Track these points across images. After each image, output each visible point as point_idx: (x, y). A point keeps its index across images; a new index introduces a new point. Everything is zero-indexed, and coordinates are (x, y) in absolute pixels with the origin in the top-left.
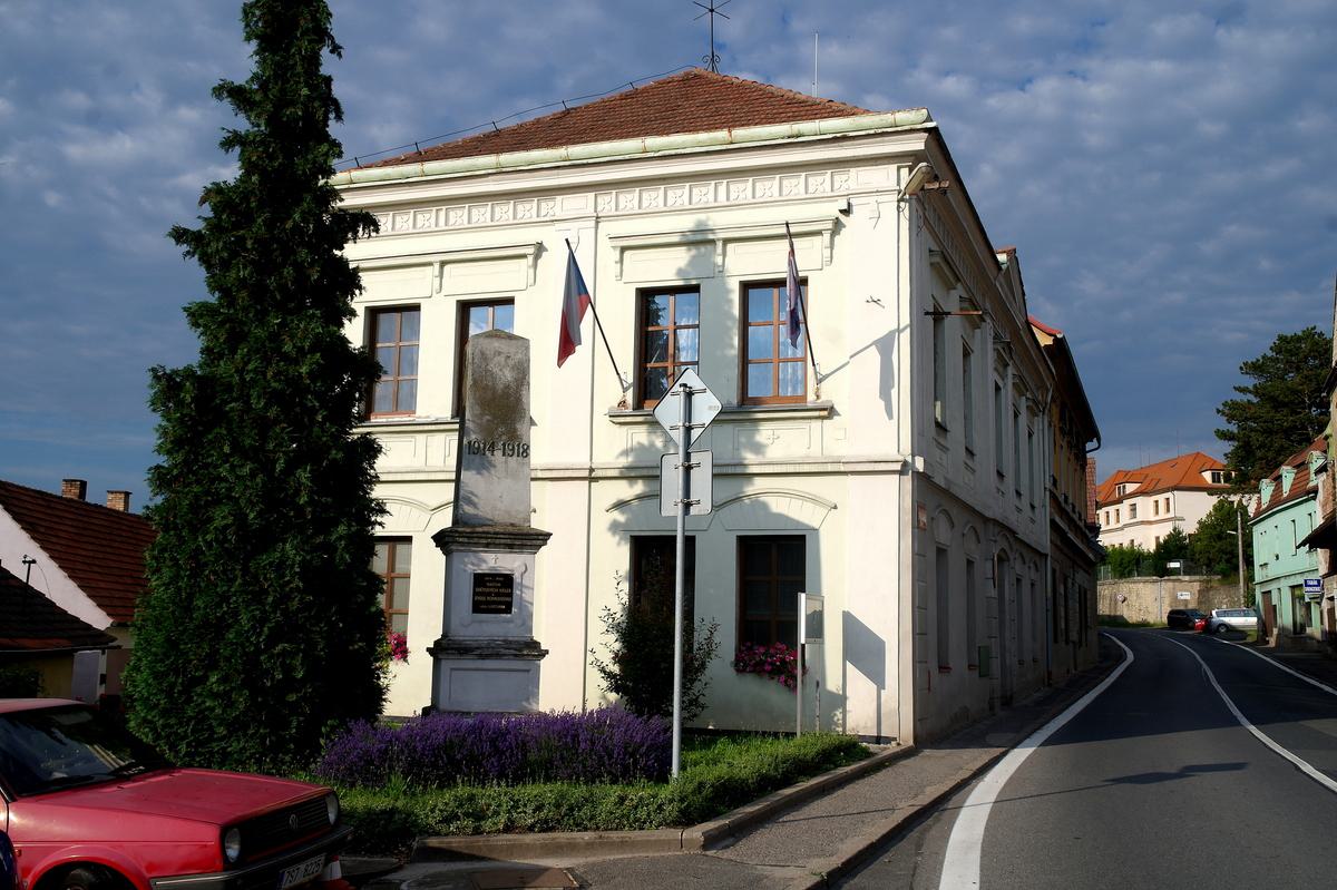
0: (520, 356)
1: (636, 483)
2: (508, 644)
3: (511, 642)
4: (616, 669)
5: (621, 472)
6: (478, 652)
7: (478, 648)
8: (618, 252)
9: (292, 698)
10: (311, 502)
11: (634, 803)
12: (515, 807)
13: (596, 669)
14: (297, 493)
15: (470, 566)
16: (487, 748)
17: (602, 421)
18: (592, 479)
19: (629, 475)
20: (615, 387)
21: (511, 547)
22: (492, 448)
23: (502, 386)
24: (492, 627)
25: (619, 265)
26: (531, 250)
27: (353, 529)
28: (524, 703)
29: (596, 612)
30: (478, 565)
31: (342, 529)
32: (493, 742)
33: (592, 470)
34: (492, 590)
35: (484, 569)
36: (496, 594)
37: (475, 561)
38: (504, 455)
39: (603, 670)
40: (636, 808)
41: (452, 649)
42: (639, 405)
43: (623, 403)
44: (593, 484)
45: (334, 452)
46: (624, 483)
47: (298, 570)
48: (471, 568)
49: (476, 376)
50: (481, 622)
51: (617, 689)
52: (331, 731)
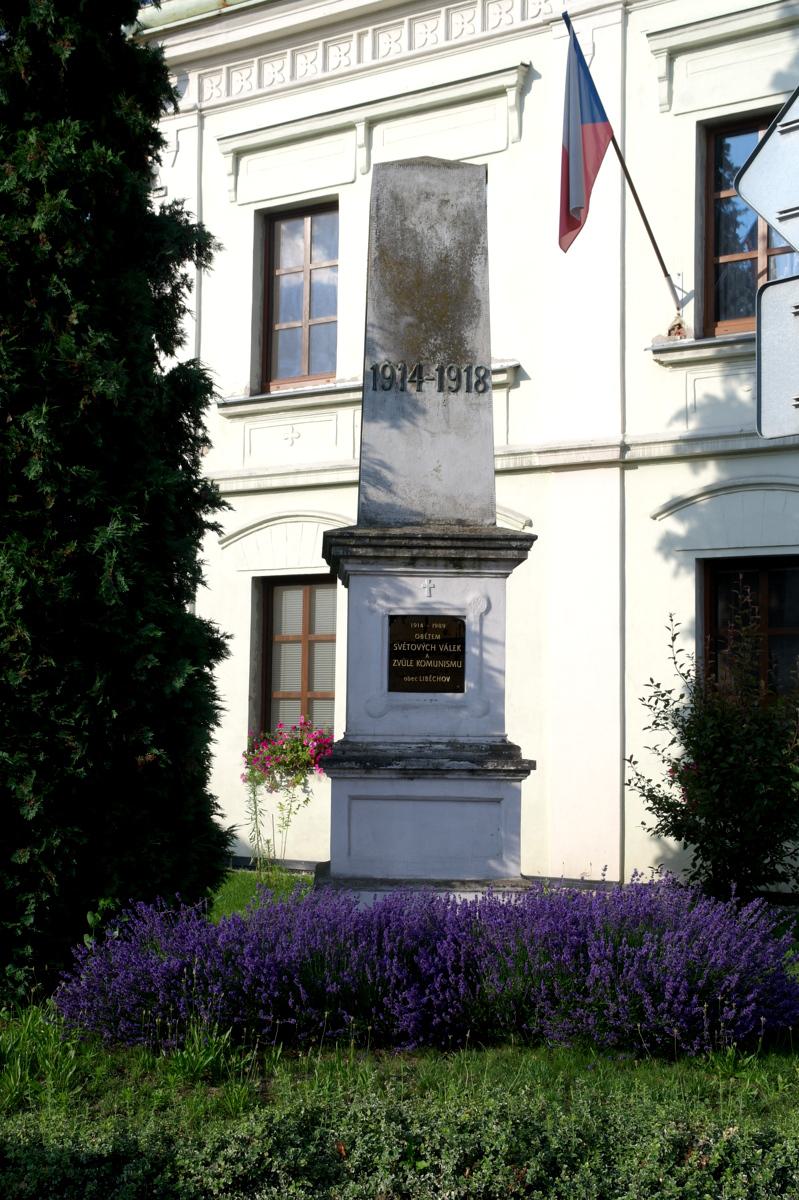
0: (466, 199)
1: (704, 466)
2: (456, 749)
3: (463, 746)
4: (675, 793)
5: (677, 449)
6: (401, 765)
7: (400, 758)
8: (663, 60)
9: (22, 857)
10: (48, 475)
11: (715, 1158)
12: (411, 1155)
13: (637, 793)
14: (24, 459)
15: (382, 602)
16: (393, 967)
17: (642, 362)
18: (626, 464)
19: (690, 452)
20: (663, 300)
21: (457, 564)
22: (419, 377)
23: (434, 259)
24: (426, 718)
25: (666, 83)
26: (512, 79)
27: (136, 528)
28: (493, 863)
29: (637, 690)
30: (397, 601)
31: (114, 528)
32: (406, 956)
33: (624, 448)
34: (424, 647)
35: (408, 607)
36: (430, 654)
37: (390, 592)
38: (441, 389)
39: (651, 796)
40: (717, 1174)
41: (349, 760)
42: (706, 329)
43: (677, 329)
44: (628, 473)
45: (101, 382)
46: (682, 469)
47: (19, 607)
48: (383, 607)
49: (385, 240)
50: (405, 708)
51: (676, 829)
52: (103, 922)
